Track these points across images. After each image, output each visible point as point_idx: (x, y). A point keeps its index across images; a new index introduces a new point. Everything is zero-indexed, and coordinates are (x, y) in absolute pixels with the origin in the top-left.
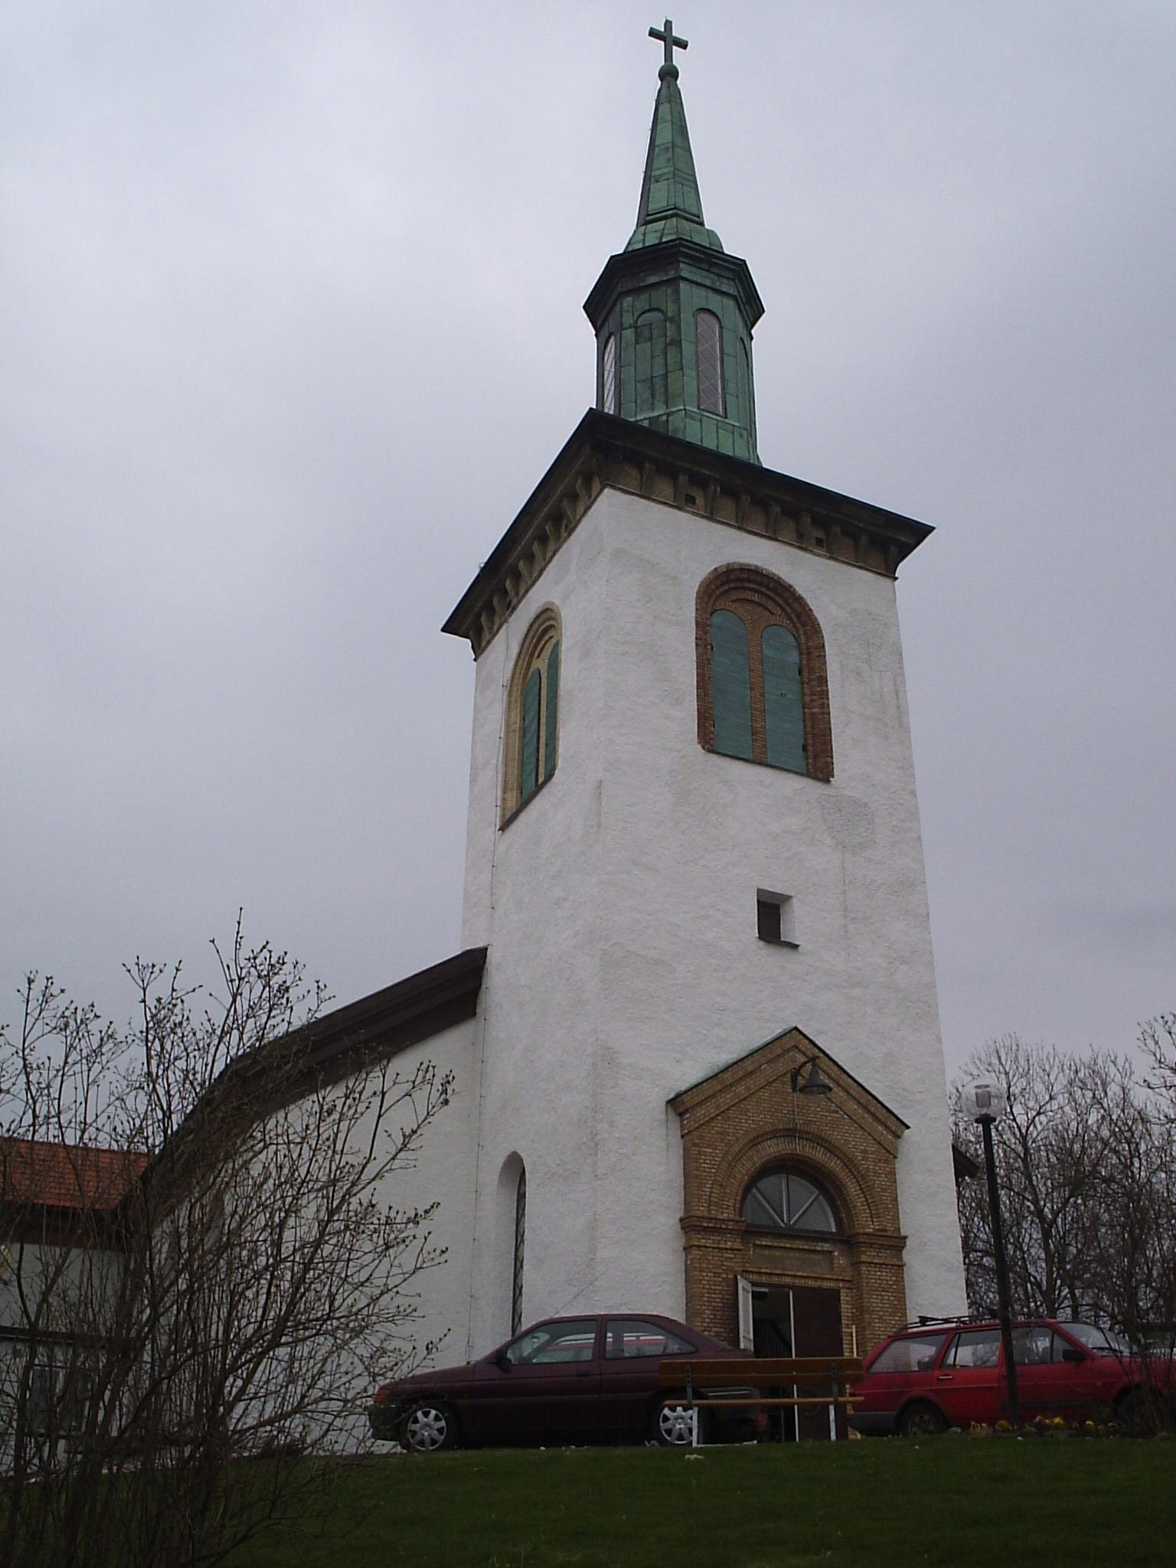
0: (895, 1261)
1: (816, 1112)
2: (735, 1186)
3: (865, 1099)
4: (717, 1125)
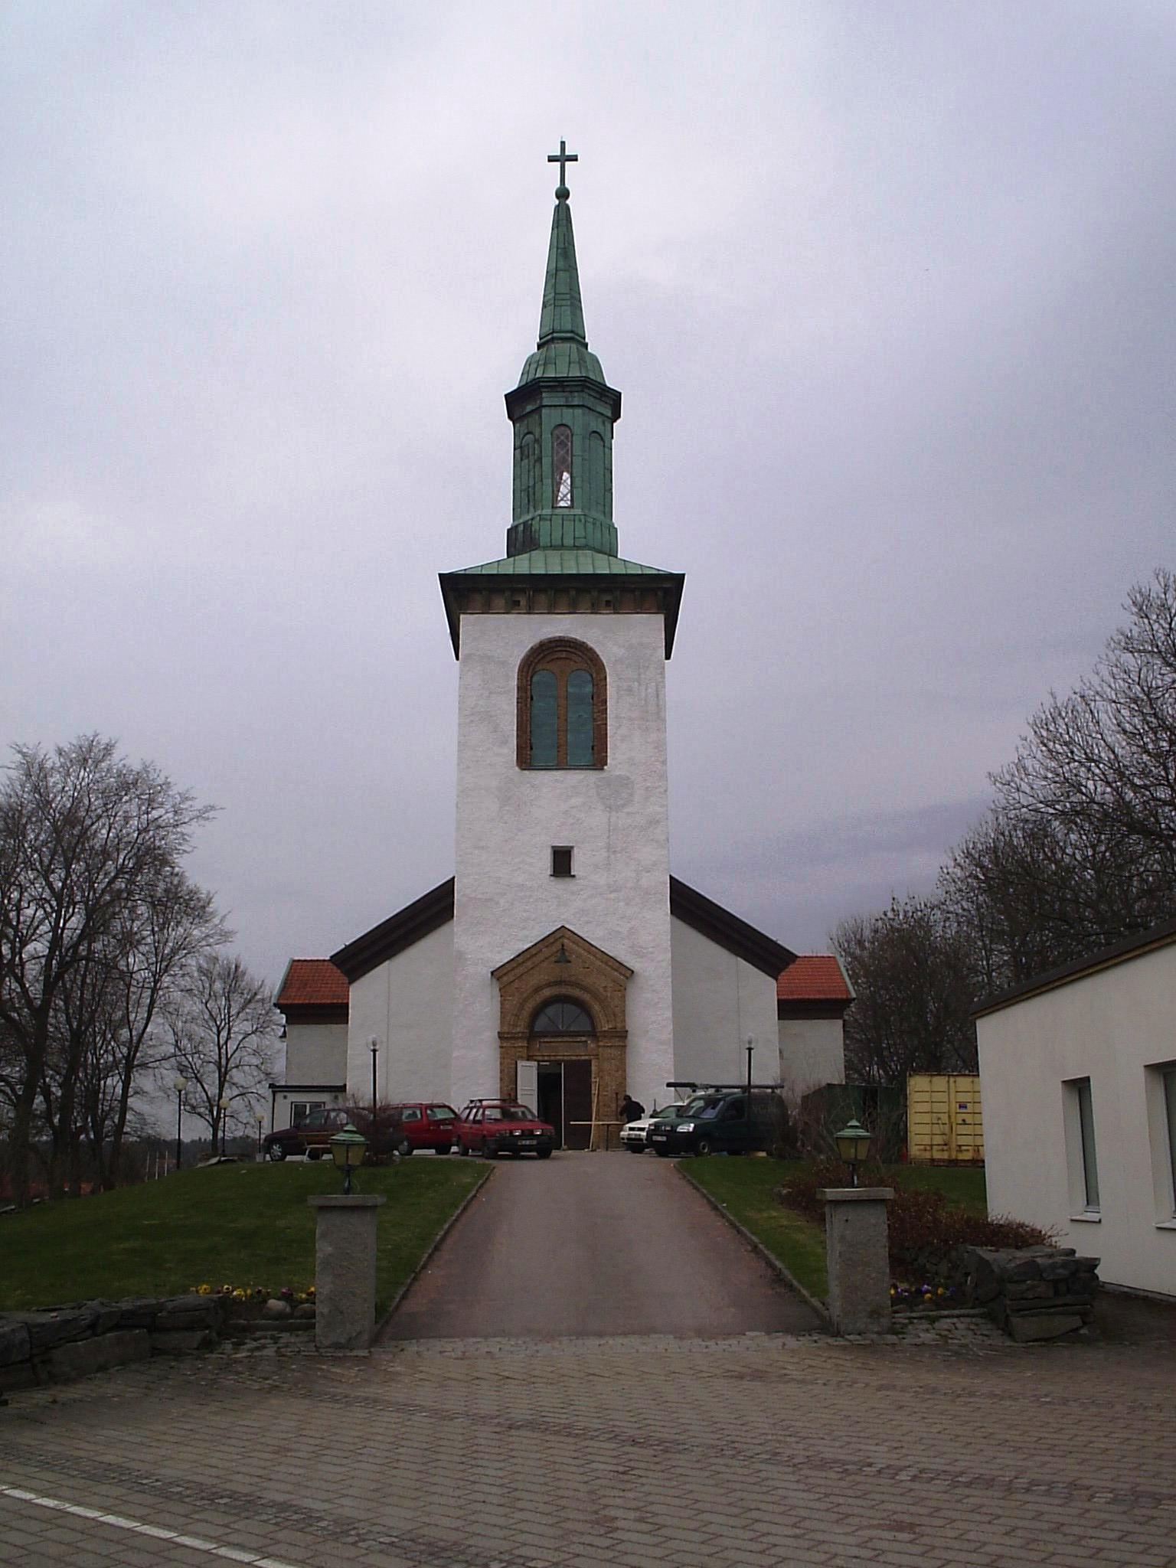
2: (526, 1014)
4: (516, 985)
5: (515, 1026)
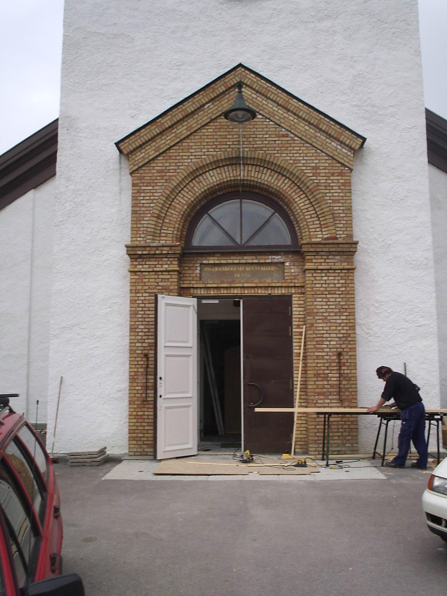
0: (345, 265)
1: (260, 136)
2: (175, 216)
3: (315, 118)
4: (158, 165)
5: (155, 235)
